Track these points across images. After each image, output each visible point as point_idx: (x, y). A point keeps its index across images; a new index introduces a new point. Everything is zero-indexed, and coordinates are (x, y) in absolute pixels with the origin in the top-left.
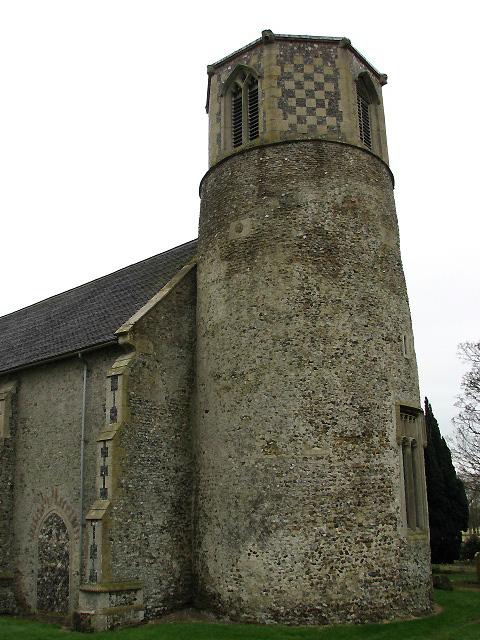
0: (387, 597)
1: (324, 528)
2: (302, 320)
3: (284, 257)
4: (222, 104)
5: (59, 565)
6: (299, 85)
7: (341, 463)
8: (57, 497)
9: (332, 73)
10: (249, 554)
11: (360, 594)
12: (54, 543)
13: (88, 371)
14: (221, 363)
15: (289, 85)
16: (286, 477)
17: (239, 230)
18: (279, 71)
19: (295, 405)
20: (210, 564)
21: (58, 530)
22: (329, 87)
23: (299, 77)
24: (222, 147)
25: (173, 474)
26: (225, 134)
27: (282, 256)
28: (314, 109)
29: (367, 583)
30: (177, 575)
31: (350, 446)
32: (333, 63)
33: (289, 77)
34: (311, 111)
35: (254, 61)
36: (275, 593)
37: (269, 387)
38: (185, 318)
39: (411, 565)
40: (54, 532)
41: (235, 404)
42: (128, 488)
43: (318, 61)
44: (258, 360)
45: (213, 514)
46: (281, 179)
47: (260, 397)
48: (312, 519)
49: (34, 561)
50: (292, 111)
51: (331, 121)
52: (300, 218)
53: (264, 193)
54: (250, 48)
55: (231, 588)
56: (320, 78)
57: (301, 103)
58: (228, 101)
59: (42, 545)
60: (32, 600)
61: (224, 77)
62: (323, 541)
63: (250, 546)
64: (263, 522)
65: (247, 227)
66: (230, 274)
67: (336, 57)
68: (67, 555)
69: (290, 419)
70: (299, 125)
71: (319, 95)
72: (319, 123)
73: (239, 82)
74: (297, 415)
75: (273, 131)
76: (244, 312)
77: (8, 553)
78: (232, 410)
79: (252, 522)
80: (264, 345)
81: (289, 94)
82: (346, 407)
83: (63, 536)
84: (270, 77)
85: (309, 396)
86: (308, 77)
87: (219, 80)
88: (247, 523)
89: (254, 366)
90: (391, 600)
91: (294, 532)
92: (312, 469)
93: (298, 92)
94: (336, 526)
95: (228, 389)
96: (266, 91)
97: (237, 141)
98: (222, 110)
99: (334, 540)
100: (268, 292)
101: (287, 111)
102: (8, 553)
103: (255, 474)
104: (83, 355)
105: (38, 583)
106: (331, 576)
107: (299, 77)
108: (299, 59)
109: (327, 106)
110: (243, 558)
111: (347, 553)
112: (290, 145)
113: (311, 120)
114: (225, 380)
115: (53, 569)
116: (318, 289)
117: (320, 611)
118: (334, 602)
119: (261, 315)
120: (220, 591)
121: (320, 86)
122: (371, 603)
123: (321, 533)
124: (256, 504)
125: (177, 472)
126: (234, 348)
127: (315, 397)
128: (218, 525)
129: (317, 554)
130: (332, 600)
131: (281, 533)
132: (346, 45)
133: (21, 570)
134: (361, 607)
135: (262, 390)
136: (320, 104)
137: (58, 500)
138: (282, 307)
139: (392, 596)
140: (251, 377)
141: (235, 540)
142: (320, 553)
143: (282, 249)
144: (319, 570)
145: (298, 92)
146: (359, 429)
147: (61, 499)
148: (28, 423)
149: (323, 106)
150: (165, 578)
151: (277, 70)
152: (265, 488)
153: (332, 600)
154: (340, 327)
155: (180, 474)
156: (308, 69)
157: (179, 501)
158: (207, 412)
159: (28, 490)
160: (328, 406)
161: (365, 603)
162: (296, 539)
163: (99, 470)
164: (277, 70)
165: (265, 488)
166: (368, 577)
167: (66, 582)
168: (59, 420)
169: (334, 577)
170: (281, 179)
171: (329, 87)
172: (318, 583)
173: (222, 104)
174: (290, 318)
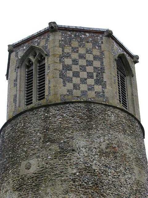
6: (75, 62)
9: (98, 54)
15: (68, 61)
22: (97, 64)
23: (75, 56)
24: (17, 105)
28: (86, 79)
32: (100, 47)
33: (68, 56)
34: (83, 81)
35: (43, 43)
43: (89, 46)
50: (70, 80)
51: (98, 88)
52: (74, 160)
54: (40, 34)
56: (90, 57)
57: (76, 74)
58: (23, 72)
61: (21, 53)
65: (35, 165)
67: (102, 43)
71: (90, 69)
72: (89, 89)
73: (31, 58)
81: (68, 68)
84: (54, 55)
86: (82, 56)
87: (17, 56)
96: (51, 66)
97: (29, 101)
107: (75, 56)
108: (75, 44)
109: (95, 78)
113: (83, 87)
121: (90, 63)
132: (109, 35)
136: (90, 76)
143: (60, 183)
149: (92, 77)
151: (59, 51)
156: (82, 51)
164: (59, 51)
170: (60, 130)
171: (97, 64)
173: (19, 74)
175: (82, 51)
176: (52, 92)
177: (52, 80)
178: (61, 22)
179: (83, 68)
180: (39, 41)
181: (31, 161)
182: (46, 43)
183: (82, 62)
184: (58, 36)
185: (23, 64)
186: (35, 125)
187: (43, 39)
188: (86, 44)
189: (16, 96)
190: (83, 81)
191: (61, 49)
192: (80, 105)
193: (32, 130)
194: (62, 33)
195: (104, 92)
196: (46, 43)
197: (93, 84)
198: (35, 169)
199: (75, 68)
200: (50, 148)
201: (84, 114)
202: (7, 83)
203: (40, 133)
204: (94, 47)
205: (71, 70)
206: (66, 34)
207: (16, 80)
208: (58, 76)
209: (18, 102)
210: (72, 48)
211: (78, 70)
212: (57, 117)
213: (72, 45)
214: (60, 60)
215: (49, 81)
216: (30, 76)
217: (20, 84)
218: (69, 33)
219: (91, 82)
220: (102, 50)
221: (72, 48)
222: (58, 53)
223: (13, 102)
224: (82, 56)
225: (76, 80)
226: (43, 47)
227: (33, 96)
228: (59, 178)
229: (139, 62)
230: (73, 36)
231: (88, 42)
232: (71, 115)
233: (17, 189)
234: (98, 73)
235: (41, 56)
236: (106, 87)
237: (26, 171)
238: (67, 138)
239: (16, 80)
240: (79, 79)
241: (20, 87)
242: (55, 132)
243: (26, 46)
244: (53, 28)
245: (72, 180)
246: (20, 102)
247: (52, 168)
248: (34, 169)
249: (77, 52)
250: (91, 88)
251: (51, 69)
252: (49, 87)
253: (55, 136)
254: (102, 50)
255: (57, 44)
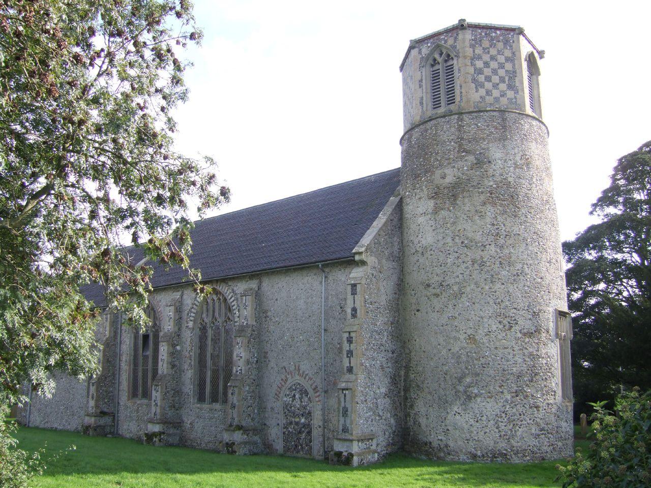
0: (549, 446)
1: (509, 397)
2: (493, 248)
3: (480, 200)
4: (424, 74)
5: (303, 420)
6: (487, 64)
7: (521, 352)
8: (299, 370)
9: (510, 55)
10: (455, 415)
11: (533, 442)
12: (297, 403)
13: (326, 277)
14: (430, 276)
15: (479, 64)
16: (483, 361)
17: (443, 178)
18: (472, 53)
19: (490, 310)
20: (423, 421)
21: (301, 394)
23: (486, 58)
24: (425, 109)
25: (390, 355)
26: (426, 97)
27: (479, 199)
28: (498, 84)
29: (537, 436)
30: (394, 429)
31: (527, 340)
32: (511, 46)
33: (479, 58)
34: (496, 86)
35: (451, 41)
36: (474, 442)
37: (470, 296)
38: (395, 239)
39: (564, 424)
40: (297, 396)
41: (443, 307)
42: (366, 366)
43: (500, 45)
44: (460, 276)
45: (425, 386)
46: (476, 140)
47: (465, 301)
48: (501, 390)
49: (279, 417)
50: (482, 86)
51: (510, 94)
52: (491, 172)
53: (463, 150)
54: (448, 31)
55: (440, 438)
56: (501, 59)
57: (488, 79)
58: (426, 72)
59: (286, 406)
60: (279, 446)
61: (425, 50)
62: (508, 406)
63: (456, 409)
64: (465, 392)
65: (450, 175)
66: (436, 211)
67: (513, 42)
68: (310, 413)
69: (485, 320)
70: (487, 97)
71: (502, 72)
72: (502, 96)
73: (437, 56)
74: (490, 317)
75: (468, 101)
76: (449, 240)
77: (256, 411)
78: (441, 311)
79: (457, 392)
80: (465, 265)
81: (480, 72)
82: (524, 311)
83: (306, 399)
84: (465, 57)
85: (499, 303)
86: (493, 58)
87: (420, 52)
88: (453, 392)
89: (457, 280)
90: (552, 447)
91: (488, 400)
92: (501, 356)
93: (486, 70)
94: (517, 396)
95: (437, 295)
96: (462, 69)
98: (424, 77)
99: (516, 405)
100: (468, 226)
101: (479, 85)
102: (256, 411)
103: (459, 357)
104: (322, 265)
105: (284, 433)
106: (513, 430)
108: (486, 43)
109: (507, 82)
110: (449, 417)
111: (524, 415)
112: (482, 114)
113: (496, 93)
114: (434, 288)
115: (297, 423)
116: (504, 225)
117: (506, 455)
118: (515, 448)
119: (462, 243)
120: (431, 440)
121: (502, 66)
122: (539, 450)
123: (507, 401)
124: (460, 380)
125: (393, 353)
126: (441, 266)
127: (503, 305)
128: (430, 393)
129: (504, 415)
130: (514, 447)
131: (479, 399)
133: (267, 423)
134: (533, 452)
135: (464, 299)
136: (502, 80)
137: (301, 372)
138: (478, 237)
139: (552, 445)
140: (456, 288)
141: (444, 403)
142: (506, 414)
143: (477, 195)
144: (505, 426)
145: (486, 70)
146: (532, 328)
147: (304, 372)
148: (269, 314)
149: (504, 82)
150: (387, 430)
151: (469, 52)
152: (466, 368)
153: (514, 447)
154: (520, 254)
155: (395, 355)
156: (493, 52)
157: (395, 374)
158: (418, 311)
159: (272, 364)
160: (512, 311)
161: (536, 449)
162: (490, 405)
163: (345, 353)
164: (469, 52)
165: (466, 368)
166: (537, 432)
167: (309, 433)
168: (299, 312)
169: (515, 431)
170: (476, 140)
171: (508, 66)
172: (504, 435)
173: (424, 74)
174: (485, 246)
175: (493, 52)
176: (464, 99)
177: (464, 85)
178: (471, 19)
179: (495, 72)
180: (446, 38)
181: (446, 171)
182: (455, 42)
183: (494, 65)
184: (468, 35)
185: (428, 62)
186: (447, 132)
187: (451, 36)
188: (497, 43)
189: (422, 98)
190: (496, 86)
191: (471, 49)
192: (495, 114)
193: (445, 138)
194: (473, 31)
195: (516, 99)
196: (455, 42)
197: (505, 89)
198: (451, 179)
199: (487, 72)
200: (466, 158)
201: (499, 123)
202: (401, 76)
203: (454, 142)
204: (505, 47)
205: (483, 74)
206: (476, 31)
207: (421, 81)
208: (470, 81)
209: (425, 105)
210: (483, 48)
211: (490, 74)
212: (471, 126)
213: (483, 46)
214: (471, 63)
215: (461, 86)
216: (435, 76)
217: (426, 84)
218: (480, 31)
219: (503, 87)
220: (514, 50)
221: (483, 48)
222: (470, 55)
223: (419, 104)
224: (493, 58)
225: (488, 85)
226: (451, 46)
227: (441, 98)
228: (476, 190)
229: (542, 49)
230: (483, 34)
231: (499, 41)
232: (486, 124)
233: (433, 197)
234: (510, 77)
235: (448, 56)
236: (518, 92)
237: (441, 180)
238: (484, 149)
239: (421, 81)
240: (491, 84)
241: (426, 88)
242: (470, 142)
243: (431, 43)
244: (462, 26)
245: (489, 192)
246: (427, 105)
247: (469, 180)
248: (449, 179)
249: (488, 52)
250: (503, 95)
251: (462, 73)
252: (461, 93)
253: (468, 147)
254: (514, 50)
255: (467, 44)
